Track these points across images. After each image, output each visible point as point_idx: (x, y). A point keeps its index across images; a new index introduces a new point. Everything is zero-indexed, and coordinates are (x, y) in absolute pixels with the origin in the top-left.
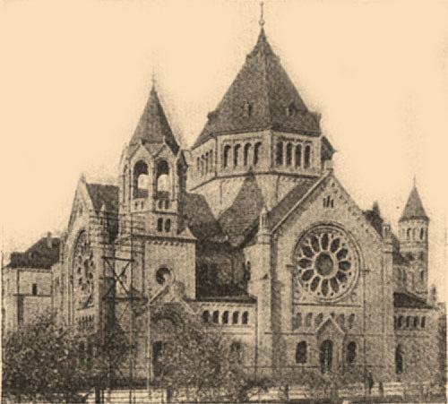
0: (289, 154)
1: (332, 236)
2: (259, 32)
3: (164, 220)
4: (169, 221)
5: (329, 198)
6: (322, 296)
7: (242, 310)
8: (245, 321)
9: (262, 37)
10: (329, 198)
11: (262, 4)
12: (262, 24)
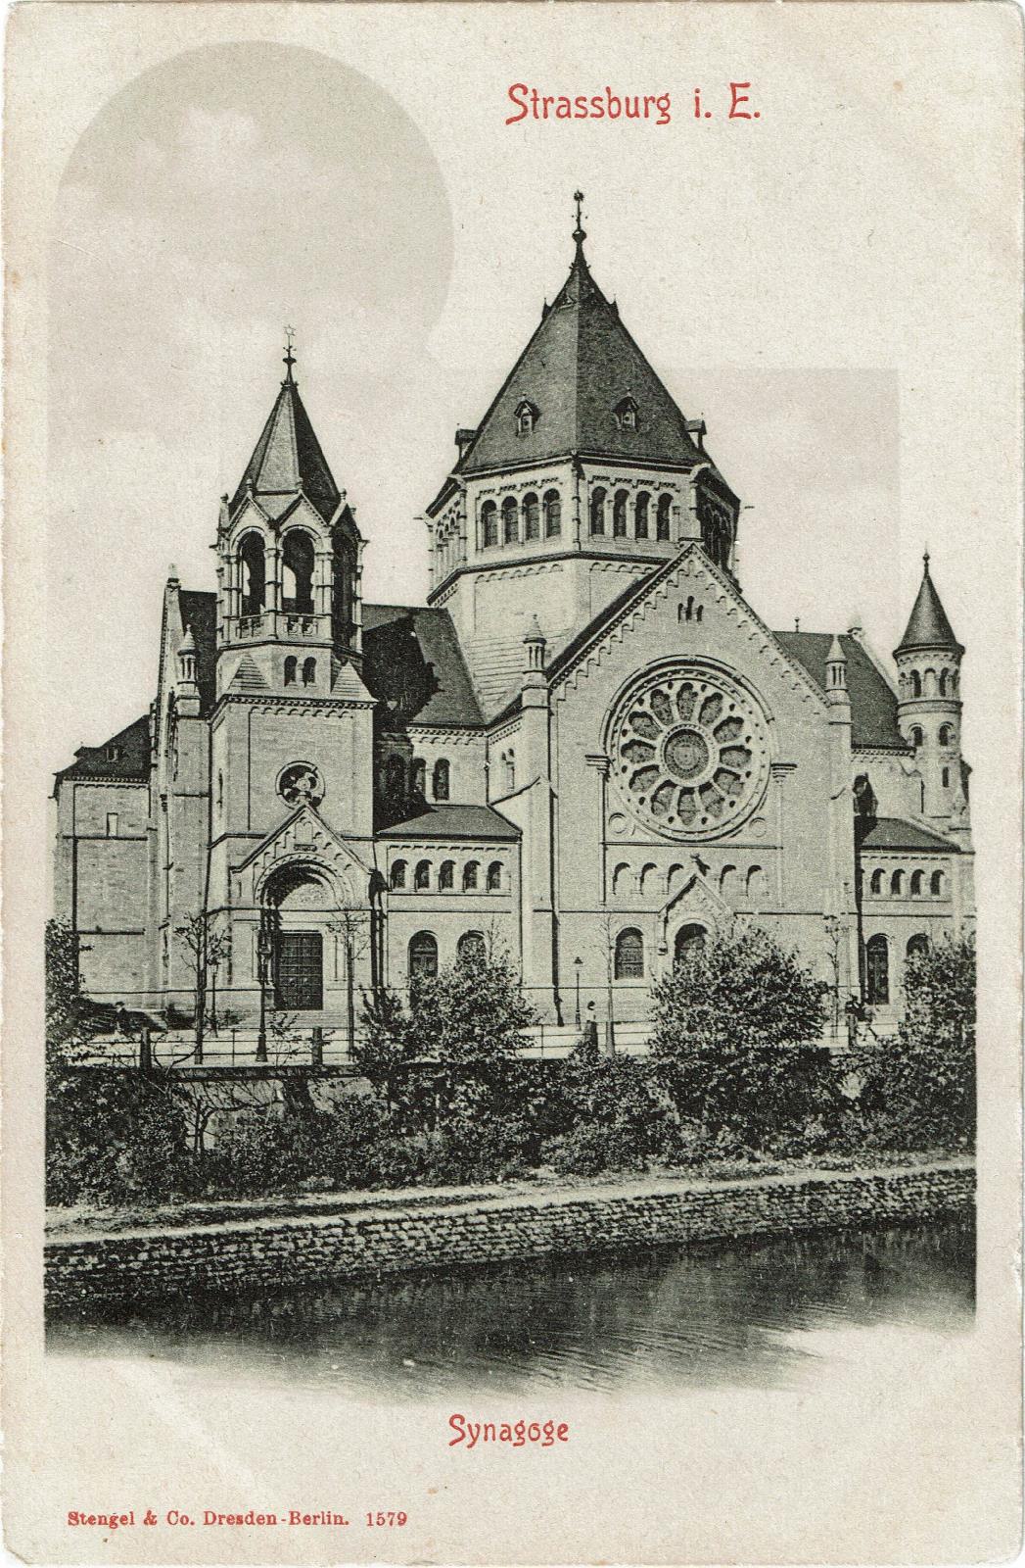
0: (618, 517)
1: (732, 707)
2: (571, 257)
3: (301, 661)
4: (310, 663)
5: (691, 600)
6: (678, 823)
7: (929, 866)
8: (492, 883)
9: (580, 265)
10: (691, 600)
11: (579, 197)
12: (580, 236)
